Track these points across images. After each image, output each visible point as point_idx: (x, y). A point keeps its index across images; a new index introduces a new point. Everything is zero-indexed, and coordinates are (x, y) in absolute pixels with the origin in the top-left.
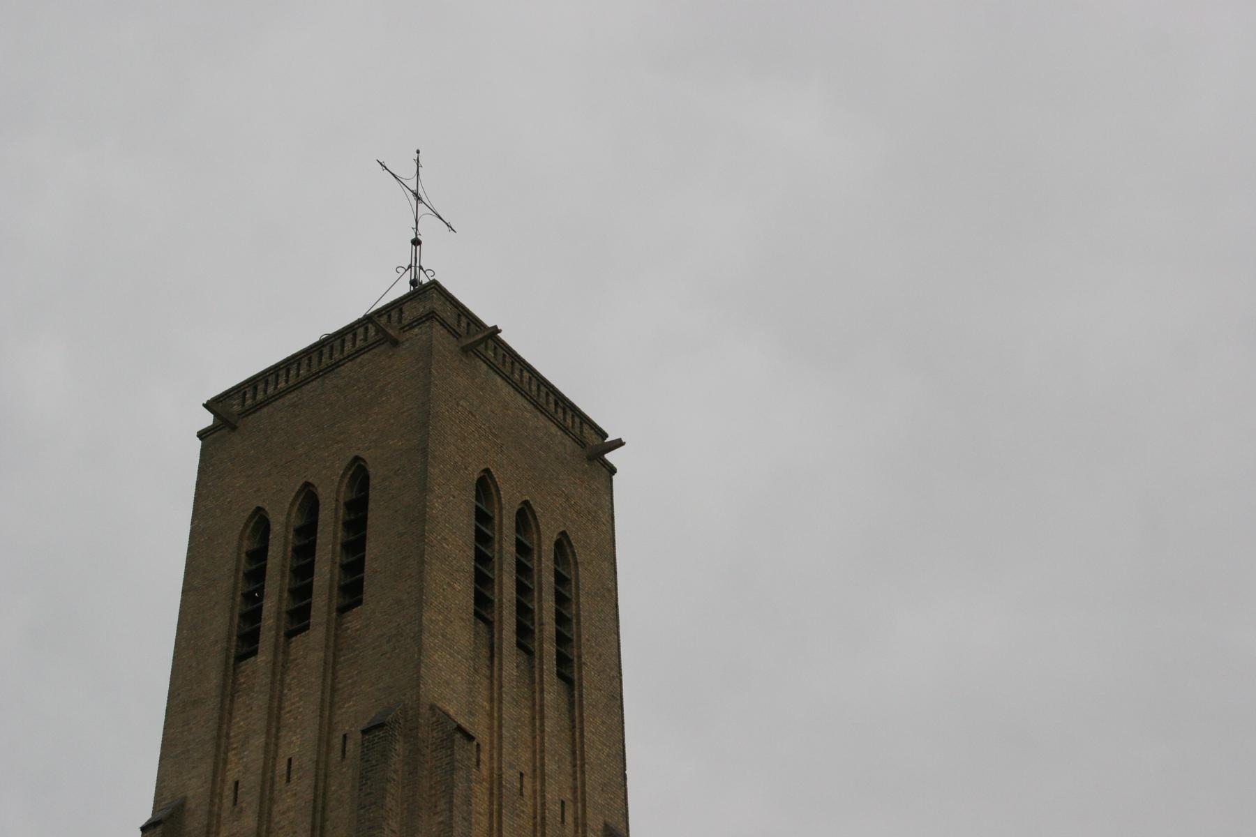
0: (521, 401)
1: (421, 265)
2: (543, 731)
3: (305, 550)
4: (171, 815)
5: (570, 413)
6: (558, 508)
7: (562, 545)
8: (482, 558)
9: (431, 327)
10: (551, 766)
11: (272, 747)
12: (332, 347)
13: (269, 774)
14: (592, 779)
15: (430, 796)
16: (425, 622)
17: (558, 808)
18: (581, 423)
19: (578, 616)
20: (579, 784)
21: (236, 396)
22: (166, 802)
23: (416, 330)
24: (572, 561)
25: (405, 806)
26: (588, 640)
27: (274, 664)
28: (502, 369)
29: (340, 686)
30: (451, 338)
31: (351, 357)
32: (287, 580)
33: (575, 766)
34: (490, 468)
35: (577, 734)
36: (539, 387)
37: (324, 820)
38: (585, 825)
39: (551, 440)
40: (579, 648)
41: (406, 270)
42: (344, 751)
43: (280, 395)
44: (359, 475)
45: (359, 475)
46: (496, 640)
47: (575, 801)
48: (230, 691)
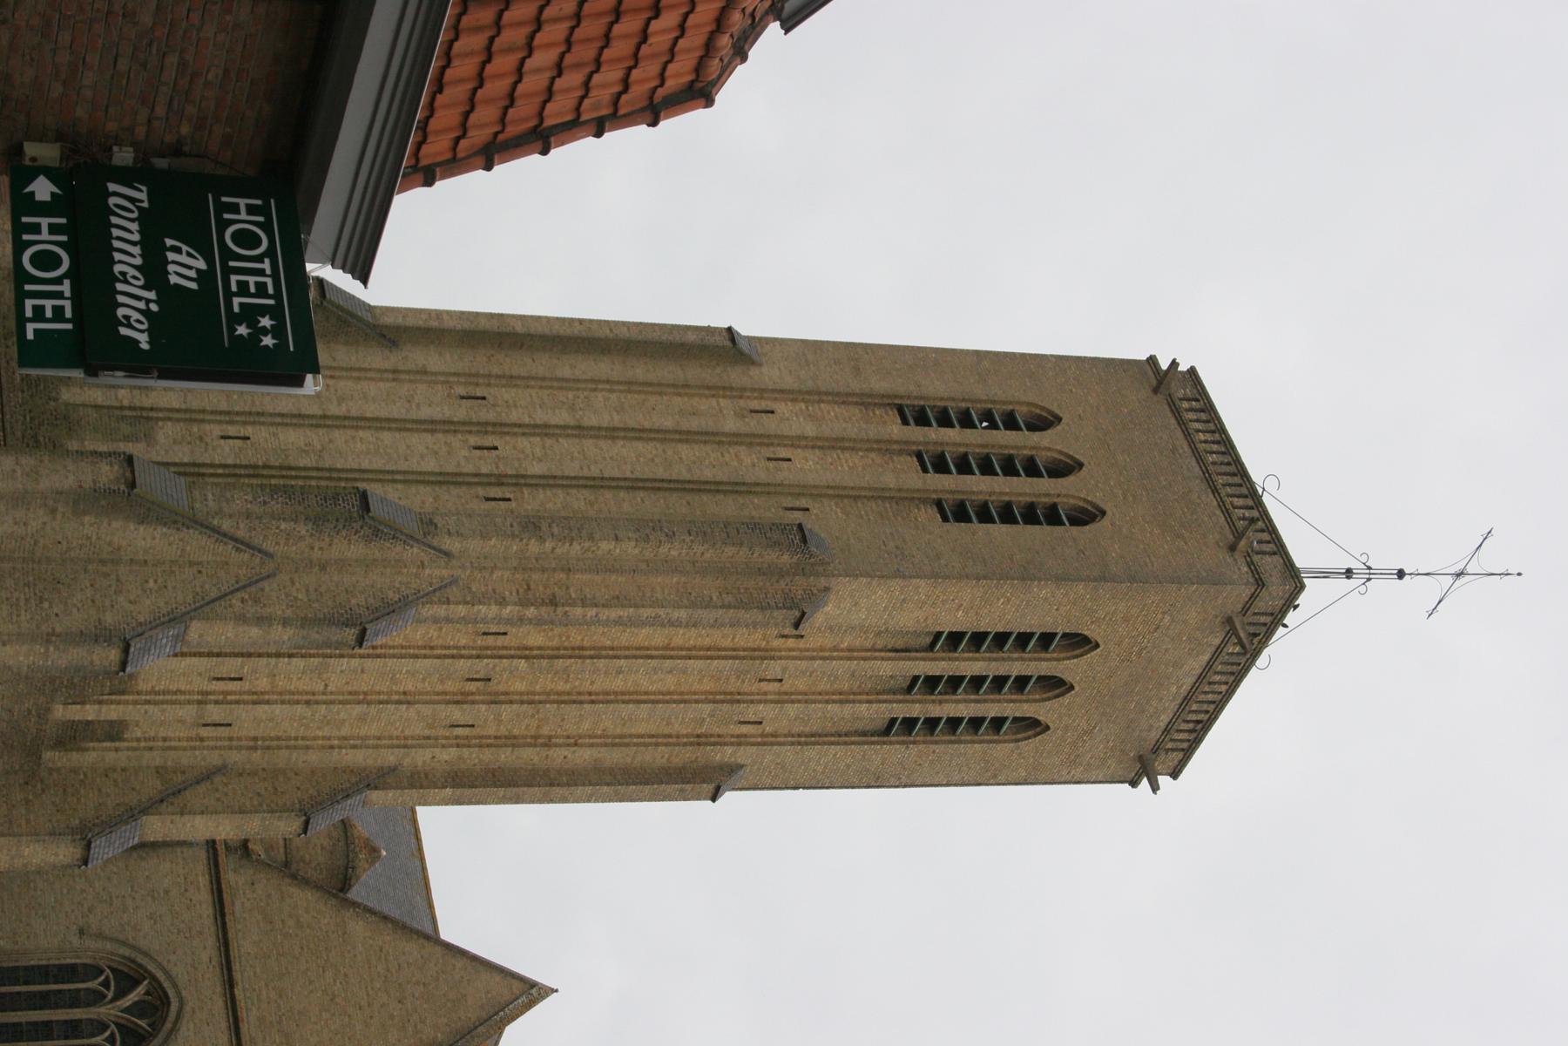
0: (1189, 681)
2: (827, 702)
4: (741, 353)
5: (1192, 737)
6: (1074, 721)
7: (1032, 726)
9: (1247, 583)
10: (792, 710)
11: (803, 443)
12: (1240, 485)
13: (776, 441)
14: (788, 753)
15: (739, 588)
16: (914, 581)
18: (1183, 750)
19: (960, 742)
20: (782, 739)
21: (1195, 391)
22: (759, 348)
23: (1246, 569)
24: (1019, 736)
25: (728, 565)
26: (934, 752)
27: (889, 442)
28: (1219, 661)
29: (860, 505)
30: (1240, 606)
31: (1222, 506)
33: (799, 736)
37: (725, 492)
38: (740, 744)
39: (1151, 716)
42: (792, 509)
43: (1187, 435)
44: (1085, 516)
45: (1085, 516)
46: (913, 654)
47: (763, 735)
48: (866, 401)
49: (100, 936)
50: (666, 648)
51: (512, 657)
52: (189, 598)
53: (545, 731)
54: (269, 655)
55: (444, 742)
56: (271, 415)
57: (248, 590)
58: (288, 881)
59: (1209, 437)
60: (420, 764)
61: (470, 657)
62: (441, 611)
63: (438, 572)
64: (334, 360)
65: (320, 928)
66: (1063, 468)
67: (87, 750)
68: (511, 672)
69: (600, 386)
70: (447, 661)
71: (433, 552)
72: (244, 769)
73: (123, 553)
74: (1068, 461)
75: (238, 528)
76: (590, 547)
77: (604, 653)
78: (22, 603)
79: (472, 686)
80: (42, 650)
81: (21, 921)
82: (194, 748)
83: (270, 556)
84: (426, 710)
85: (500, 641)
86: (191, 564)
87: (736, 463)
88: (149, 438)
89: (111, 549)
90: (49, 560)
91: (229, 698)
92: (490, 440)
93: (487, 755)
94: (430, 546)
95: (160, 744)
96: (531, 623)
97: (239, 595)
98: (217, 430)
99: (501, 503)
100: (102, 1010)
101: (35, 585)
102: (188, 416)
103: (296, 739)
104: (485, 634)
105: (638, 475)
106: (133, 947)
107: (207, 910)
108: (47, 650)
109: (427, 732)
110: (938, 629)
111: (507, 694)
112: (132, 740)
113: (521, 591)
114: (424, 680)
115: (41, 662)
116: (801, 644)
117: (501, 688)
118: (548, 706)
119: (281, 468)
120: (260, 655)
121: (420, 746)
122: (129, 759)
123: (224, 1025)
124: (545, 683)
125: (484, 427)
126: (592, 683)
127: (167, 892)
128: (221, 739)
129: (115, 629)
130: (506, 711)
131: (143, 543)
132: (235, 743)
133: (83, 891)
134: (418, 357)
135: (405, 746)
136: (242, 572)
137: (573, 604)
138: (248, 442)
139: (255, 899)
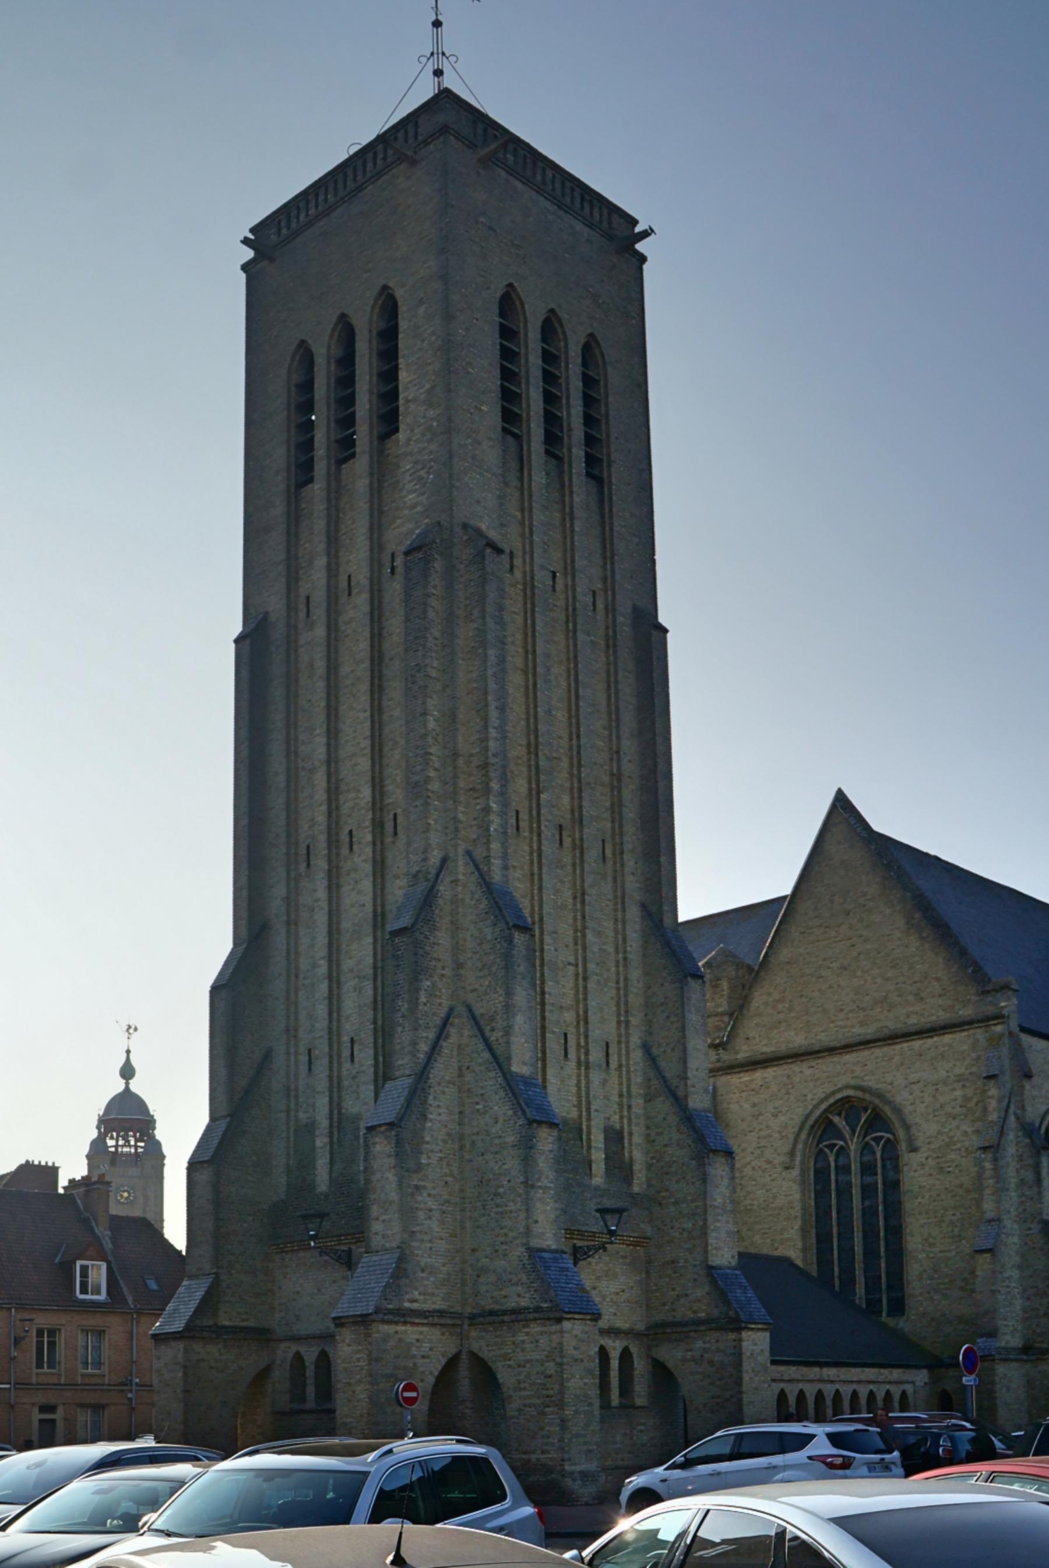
0: (544, 203)
1: (444, 50)
2: (572, 531)
3: (346, 381)
7: (590, 349)
8: (508, 375)
10: (580, 563)
12: (355, 168)
17: (589, 599)
18: (610, 214)
19: (607, 414)
23: (431, 146)
24: (600, 362)
29: (386, 509)
32: (333, 412)
34: (514, 282)
35: (607, 528)
36: (563, 183)
38: (614, 610)
40: (608, 447)
41: (429, 59)
43: (310, 224)
44: (389, 306)
46: (525, 452)
47: (605, 591)
48: (295, 517)
49: (792, 1154)
50: (525, 672)
51: (538, 805)
52: (492, 1074)
53: (606, 779)
54: (543, 1010)
55: (618, 865)
56: (330, 1022)
57: (483, 1027)
58: (745, 1011)
59: (312, 204)
60: (638, 885)
61: (540, 842)
62: (496, 863)
63: (461, 868)
64: (280, 975)
65: (785, 983)
66: (346, 332)
67: (631, 1158)
68: (553, 806)
69: (293, 749)
70: (544, 861)
71: (443, 873)
72: (646, 1031)
73: (454, 1131)
74: (339, 329)
75: (427, 1038)
76: (433, 737)
77: (532, 726)
78: (500, 1210)
79: (567, 842)
80: (541, 1191)
81: (779, 1214)
82: (628, 1072)
83: (451, 1010)
84: (589, 879)
85: (524, 816)
86: (461, 1075)
87: (354, 624)
88: (358, 1117)
89: (450, 1142)
90: (462, 1191)
91: (583, 1044)
92: (344, 837)
93: (630, 829)
94: (438, 875)
95: (625, 1100)
96: (505, 786)
97: (487, 1034)
98: (347, 1065)
99: (398, 821)
100: (852, 1148)
101: (484, 1200)
102: (335, 1090)
103: (618, 989)
104: (518, 829)
105: (368, 707)
106: (801, 1128)
107: (770, 1072)
108: (540, 1187)
109: (610, 879)
110: (499, 429)
111: (572, 812)
112: (622, 1122)
113: (476, 795)
114: (562, 882)
115: (552, 1192)
116: (518, 553)
117: (568, 816)
118: (583, 775)
119: (375, 1009)
120: (543, 1018)
121: (623, 887)
122: (637, 1124)
123: (866, 1053)
124: (562, 777)
125: (333, 841)
126: (560, 737)
127: (754, 1105)
128: (620, 1050)
129: (520, 1133)
130: (589, 810)
131: (443, 1115)
132: (623, 1039)
133: (753, 1169)
134: (276, 905)
135: (623, 898)
136: (466, 1033)
137: (486, 749)
138: (355, 1038)
139: (760, 1036)
